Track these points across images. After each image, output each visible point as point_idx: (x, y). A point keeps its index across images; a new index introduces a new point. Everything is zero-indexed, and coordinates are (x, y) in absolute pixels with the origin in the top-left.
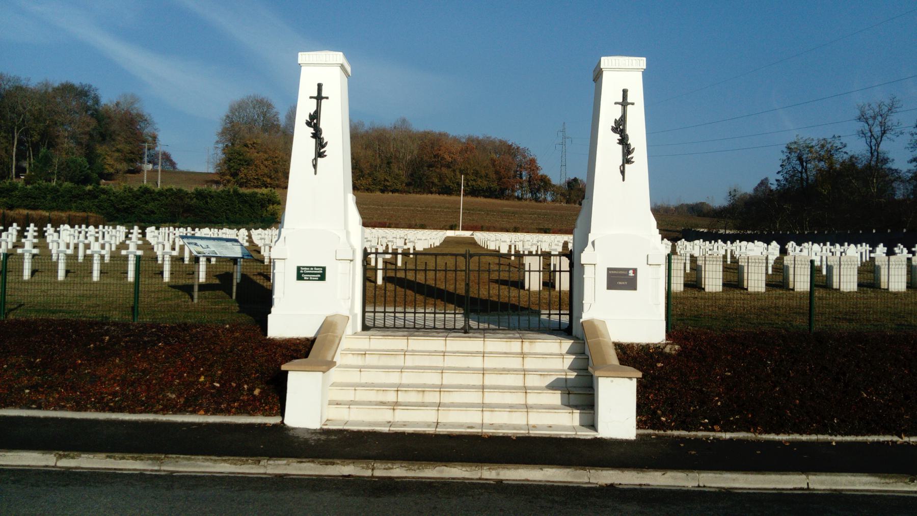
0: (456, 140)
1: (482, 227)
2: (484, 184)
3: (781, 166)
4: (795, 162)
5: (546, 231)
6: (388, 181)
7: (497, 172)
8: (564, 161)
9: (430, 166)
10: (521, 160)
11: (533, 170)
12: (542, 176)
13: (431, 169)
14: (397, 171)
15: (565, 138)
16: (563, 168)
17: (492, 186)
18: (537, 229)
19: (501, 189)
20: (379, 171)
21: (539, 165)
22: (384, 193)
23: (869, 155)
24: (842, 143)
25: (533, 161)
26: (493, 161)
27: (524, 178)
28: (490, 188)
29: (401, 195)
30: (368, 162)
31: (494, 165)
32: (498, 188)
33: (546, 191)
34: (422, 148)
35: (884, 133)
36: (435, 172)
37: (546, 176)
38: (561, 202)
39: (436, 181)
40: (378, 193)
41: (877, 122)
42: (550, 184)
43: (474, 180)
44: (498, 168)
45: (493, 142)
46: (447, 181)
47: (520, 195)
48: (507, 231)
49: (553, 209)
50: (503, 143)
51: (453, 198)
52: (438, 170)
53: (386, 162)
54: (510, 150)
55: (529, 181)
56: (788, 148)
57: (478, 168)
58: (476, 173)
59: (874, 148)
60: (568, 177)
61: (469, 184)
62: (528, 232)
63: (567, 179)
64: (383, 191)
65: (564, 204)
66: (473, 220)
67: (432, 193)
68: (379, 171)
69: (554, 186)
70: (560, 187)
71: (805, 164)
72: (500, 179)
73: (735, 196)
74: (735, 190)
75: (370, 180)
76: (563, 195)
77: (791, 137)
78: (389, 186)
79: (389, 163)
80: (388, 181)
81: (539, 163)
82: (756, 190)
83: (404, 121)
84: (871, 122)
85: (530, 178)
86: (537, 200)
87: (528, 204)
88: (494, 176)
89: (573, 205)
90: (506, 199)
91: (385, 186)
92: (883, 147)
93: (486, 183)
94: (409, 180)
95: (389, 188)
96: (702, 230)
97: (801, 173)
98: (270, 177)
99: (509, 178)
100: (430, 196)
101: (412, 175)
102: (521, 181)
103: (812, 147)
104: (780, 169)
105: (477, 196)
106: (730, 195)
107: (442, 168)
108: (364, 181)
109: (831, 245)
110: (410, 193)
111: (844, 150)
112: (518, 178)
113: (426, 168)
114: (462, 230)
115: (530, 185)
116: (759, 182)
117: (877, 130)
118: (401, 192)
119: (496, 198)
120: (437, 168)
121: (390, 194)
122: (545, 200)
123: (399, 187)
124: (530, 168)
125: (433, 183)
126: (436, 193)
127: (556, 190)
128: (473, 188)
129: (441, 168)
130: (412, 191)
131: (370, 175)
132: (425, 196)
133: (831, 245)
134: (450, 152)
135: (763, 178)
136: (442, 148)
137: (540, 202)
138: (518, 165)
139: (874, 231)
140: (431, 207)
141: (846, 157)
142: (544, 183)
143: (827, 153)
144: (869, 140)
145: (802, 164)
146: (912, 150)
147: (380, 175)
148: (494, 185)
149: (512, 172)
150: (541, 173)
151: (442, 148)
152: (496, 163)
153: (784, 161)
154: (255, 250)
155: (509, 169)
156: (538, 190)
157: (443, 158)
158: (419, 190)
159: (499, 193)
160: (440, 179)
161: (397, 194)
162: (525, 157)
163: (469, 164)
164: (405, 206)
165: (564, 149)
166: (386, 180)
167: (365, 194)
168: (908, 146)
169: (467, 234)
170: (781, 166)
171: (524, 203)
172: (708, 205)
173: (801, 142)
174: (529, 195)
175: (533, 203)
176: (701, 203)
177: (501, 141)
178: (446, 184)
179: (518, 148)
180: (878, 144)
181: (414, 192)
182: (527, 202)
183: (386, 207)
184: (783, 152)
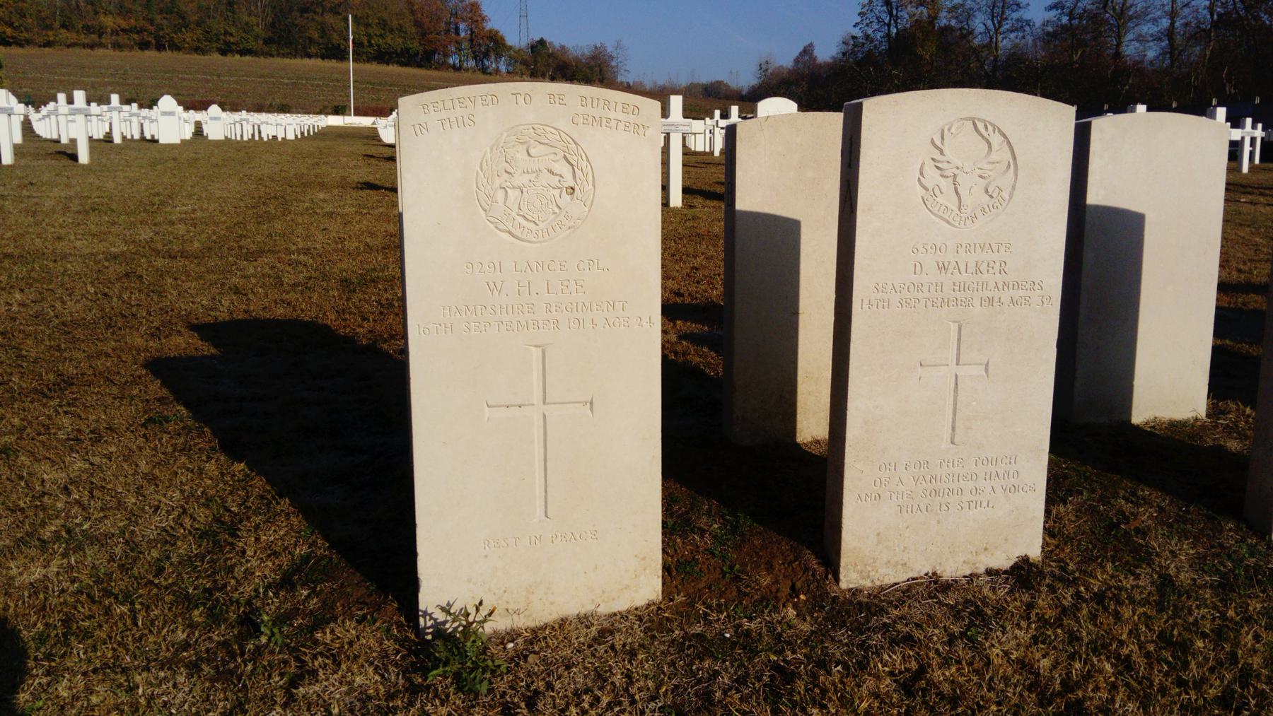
3: (859, 14)
6: (231, 35)
7: (417, 24)
11: (477, 21)
12: (491, 31)
13: (305, 15)
17: (411, 46)
19: (425, 52)
20: (214, 18)
21: (485, 14)
22: (226, 55)
27: (463, 35)
28: (408, 50)
29: (257, 59)
31: (413, 12)
33: (498, 56)
36: (313, 20)
37: (497, 32)
38: (523, 74)
39: (316, 36)
40: (216, 57)
42: (504, 45)
43: (381, 35)
44: (419, 15)
46: (335, 36)
47: (457, 61)
52: (317, 18)
55: (471, 40)
58: (383, 24)
60: (530, 37)
64: (224, 53)
66: (379, 99)
67: (310, 56)
70: (520, 50)
71: (895, 12)
72: (424, 35)
73: (767, 70)
75: (199, 31)
76: (525, 63)
78: (233, 43)
80: (231, 35)
82: (797, 61)
85: (471, 34)
88: (413, 30)
90: (436, 68)
91: (227, 43)
93: (401, 40)
97: (889, 25)
98: (11, 25)
99: (437, 34)
100: (306, 61)
101: (273, 25)
102: (458, 39)
104: (859, 19)
106: (761, 69)
107: (325, 14)
108: (189, 35)
110: (272, 56)
114: (355, 115)
116: (801, 49)
119: (419, 66)
121: (237, 57)
123: (252, 44)
124: (471, 18)
126: (317, 56)
128: (379, 49)
129: (322, 15)
131: (198, 24)
137: (490, 74)
138: (452, 14)
139: (1257, 101)
140: (307, 79)
145: (890, 13)
147: (218, 25)
148: (415, 45)
150: (489, 26)
152: (416, 7)
153: (864, 6)
154: (939, 162)
156: (486, 55)
158: (286, 50)
160: (323, 32)
161: (248, 58)
164: (260, 77)
166: (226, 33)
169: (366, 122)
170: (859, 14)
172: (726, 85)
174: (472, 63)
176: (718, 82)
178: (334, 41)
181: (278, 55)
183: (227, 78)
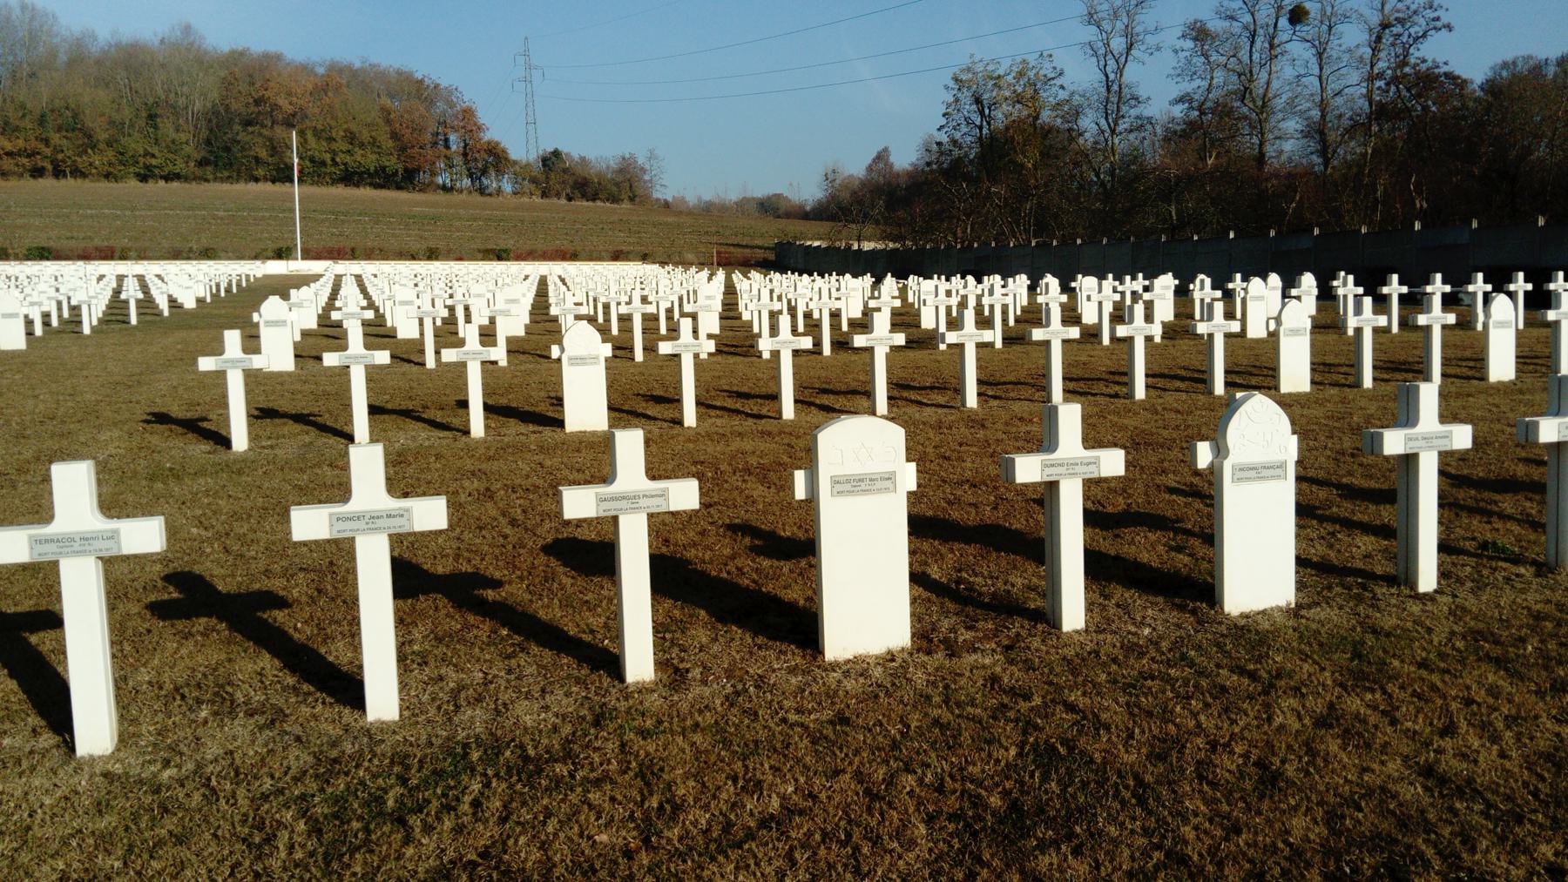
0: (305, 69)
1: (353, 250)
2: (370, 160)
4: (969, 108)
5: (501, 255)
6: (153, 156)
7: (395, 136)
8: (531, 113)
9: (248, 123)
10: (444, 112)
12: (489, 143)
14: (172, 134)
15: (529, 67)
16: (531, 127)
17: (387, 164)
18: (479, 251)
19: (406, 170)
20: (130, 135)
23: (1103, 90)
24: (1055, 68)
25: (468, 113)
26: (386, 112)
27: (454, 148)
28: (383, 168)
30: (104, 115)
31: (388, 122)
32: (400, 167)
34: (227, 84)
35: (1130, 48)
37: (497, 144)
39: (263, 154)
40: (133, 183)
41: (1119, 25)
42: (507, 159)
45: (381, 75)
47: (448, 181)
48: (413, 258)
49: (516, 209)
50: (405, 78)
51: (279, 188)
52: (265, 132)
53: (144, 114)
54: (419, 91)
56: (956, 80)
57: (354, 128)
58: (351, 137)
59: (1112, 76)
61: (338, 160)
62: (460, 259)
63: (541, 152)
64: (143, 178)
65: (537, 200)
67: (257, 180)
68: (130, 135)
69: (515, 163)
70: (528, 165)
72: (403, 149)
74: (834, 171)
75: (110, 153)
76: (534, 181)
77: (958, 58)
79: (152, 117)
80: (153, 156)
81: (483, 117)
82: (870, 169)
83: (187, 29)
84: (1106, 26)
85: (465, 147)
86: (482, 191)
87: (465, 200)
88: (390, 143)
89: (555, 200)
92: (1132, 73)
93: (374, 157)
94: (203, 153)
95: (156, 171)
96: (816, 244)
97: (981, 128)
101: (208, 142)
102: (448, 153)
103: (999, 77)
104: (943, 121)
105: (357, 185)
109: (1114, 279)
110: (207, 180)
111: (1058, 82)
112: (442, 148)
113: (237, 127)
115: (466, 162)
116: (874, 155)
117: (1118, 44)
118: (186, 179)
119: (399, 188)
120: (263, 126)
121: (162, 183)
122: (499, 191)
123: (180, 167)
124: (463, 127)
125: (257, 159)
126: (266, 179)
127: (522, 173)
130: (210, 177)
131: (109, 144)
132: (241, 187)
133: (1114, 279)
134: (289, 94)
135: (880, 149)
136: (271, 84)
137: (490, 195)
141: (1063, 95)
142: (496, 158)
143: (1029, 92)
144: (1102, 63)
145: (982, 113)
146: (1179, 79)
147: (135, 144)
148: (392, 163)
149: (429, 137)
150: (487, 136)
151: (271, 84)
153: (949, 105)
155: (421, 130)
156: (484, 172)
157: (276, 107)
158: (226, 174)
159: (407, 179)
161: (175, 184)
162: (451, 105)
163: (335, 118)
165: (529, 90)
166: (147, 154)
167: (97, 184)
168: (1172, 72)
170: (944, 115)
171: (455, 197)
173: (979, 68)
174: (467, 182)
175: (477, 198)
177: (399, 73)
179: (437, 86)
180: (1120, 71)
181: (215, 179)
182: (464, 196)
184: (947, 87)
